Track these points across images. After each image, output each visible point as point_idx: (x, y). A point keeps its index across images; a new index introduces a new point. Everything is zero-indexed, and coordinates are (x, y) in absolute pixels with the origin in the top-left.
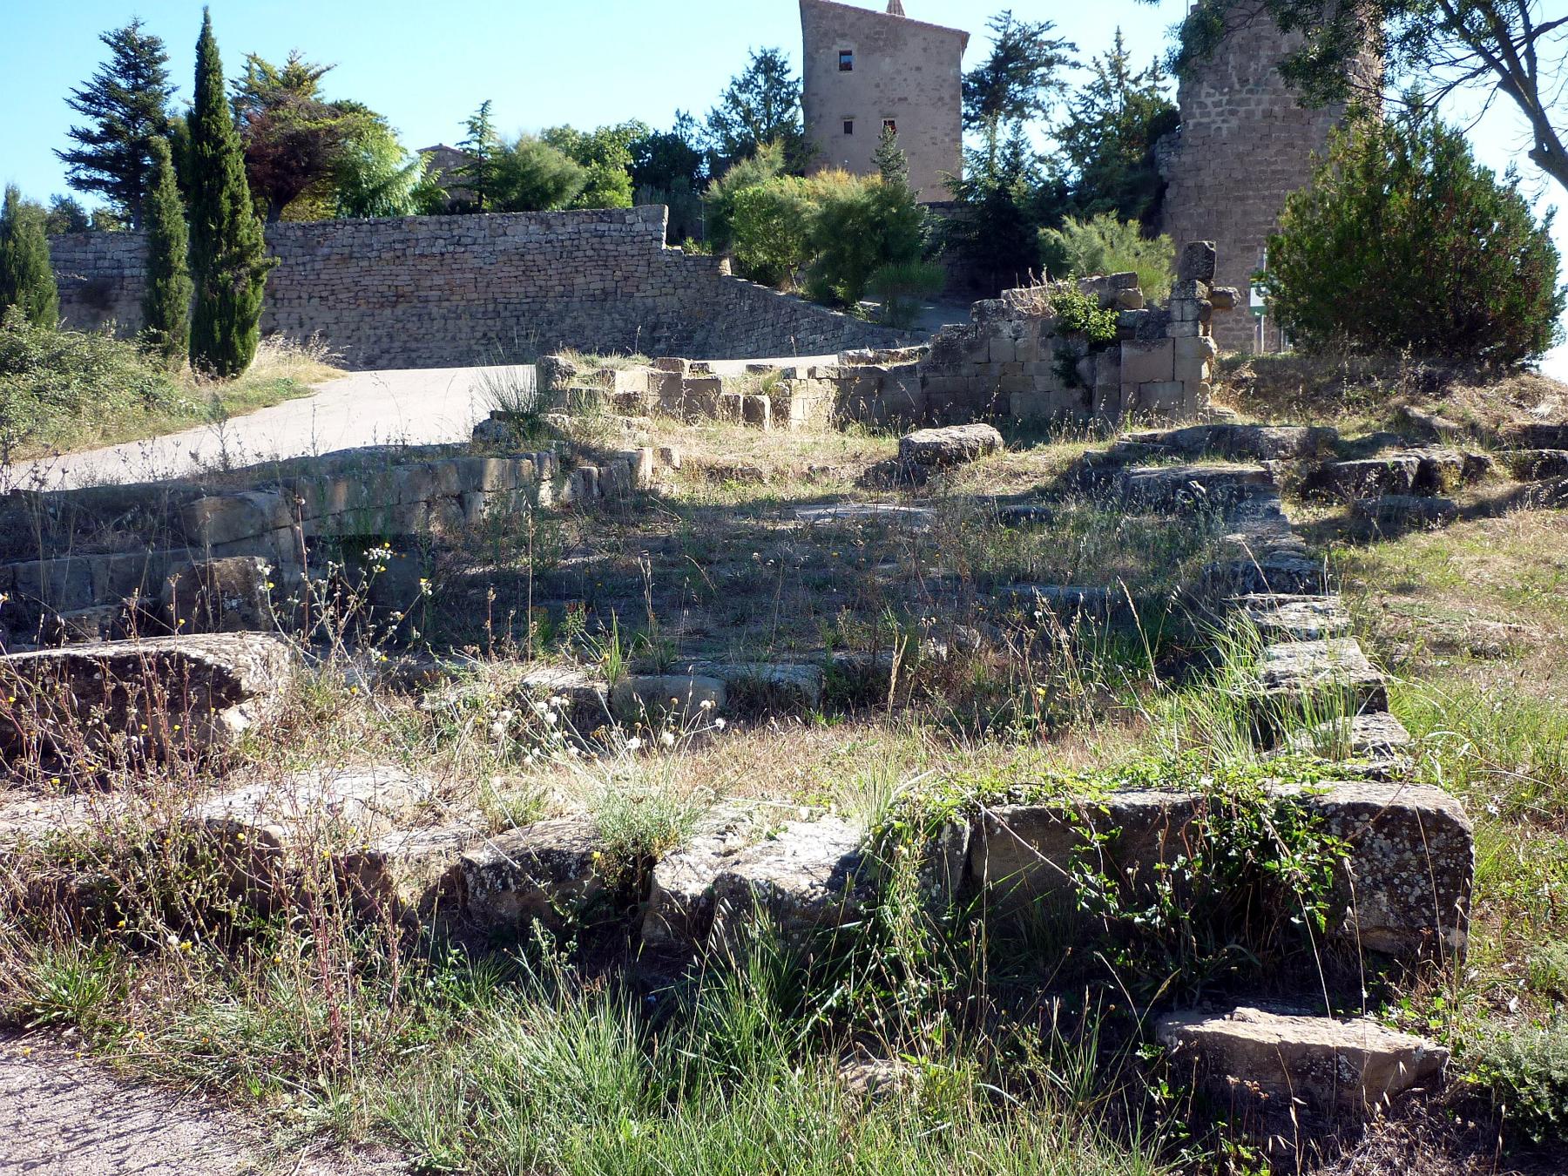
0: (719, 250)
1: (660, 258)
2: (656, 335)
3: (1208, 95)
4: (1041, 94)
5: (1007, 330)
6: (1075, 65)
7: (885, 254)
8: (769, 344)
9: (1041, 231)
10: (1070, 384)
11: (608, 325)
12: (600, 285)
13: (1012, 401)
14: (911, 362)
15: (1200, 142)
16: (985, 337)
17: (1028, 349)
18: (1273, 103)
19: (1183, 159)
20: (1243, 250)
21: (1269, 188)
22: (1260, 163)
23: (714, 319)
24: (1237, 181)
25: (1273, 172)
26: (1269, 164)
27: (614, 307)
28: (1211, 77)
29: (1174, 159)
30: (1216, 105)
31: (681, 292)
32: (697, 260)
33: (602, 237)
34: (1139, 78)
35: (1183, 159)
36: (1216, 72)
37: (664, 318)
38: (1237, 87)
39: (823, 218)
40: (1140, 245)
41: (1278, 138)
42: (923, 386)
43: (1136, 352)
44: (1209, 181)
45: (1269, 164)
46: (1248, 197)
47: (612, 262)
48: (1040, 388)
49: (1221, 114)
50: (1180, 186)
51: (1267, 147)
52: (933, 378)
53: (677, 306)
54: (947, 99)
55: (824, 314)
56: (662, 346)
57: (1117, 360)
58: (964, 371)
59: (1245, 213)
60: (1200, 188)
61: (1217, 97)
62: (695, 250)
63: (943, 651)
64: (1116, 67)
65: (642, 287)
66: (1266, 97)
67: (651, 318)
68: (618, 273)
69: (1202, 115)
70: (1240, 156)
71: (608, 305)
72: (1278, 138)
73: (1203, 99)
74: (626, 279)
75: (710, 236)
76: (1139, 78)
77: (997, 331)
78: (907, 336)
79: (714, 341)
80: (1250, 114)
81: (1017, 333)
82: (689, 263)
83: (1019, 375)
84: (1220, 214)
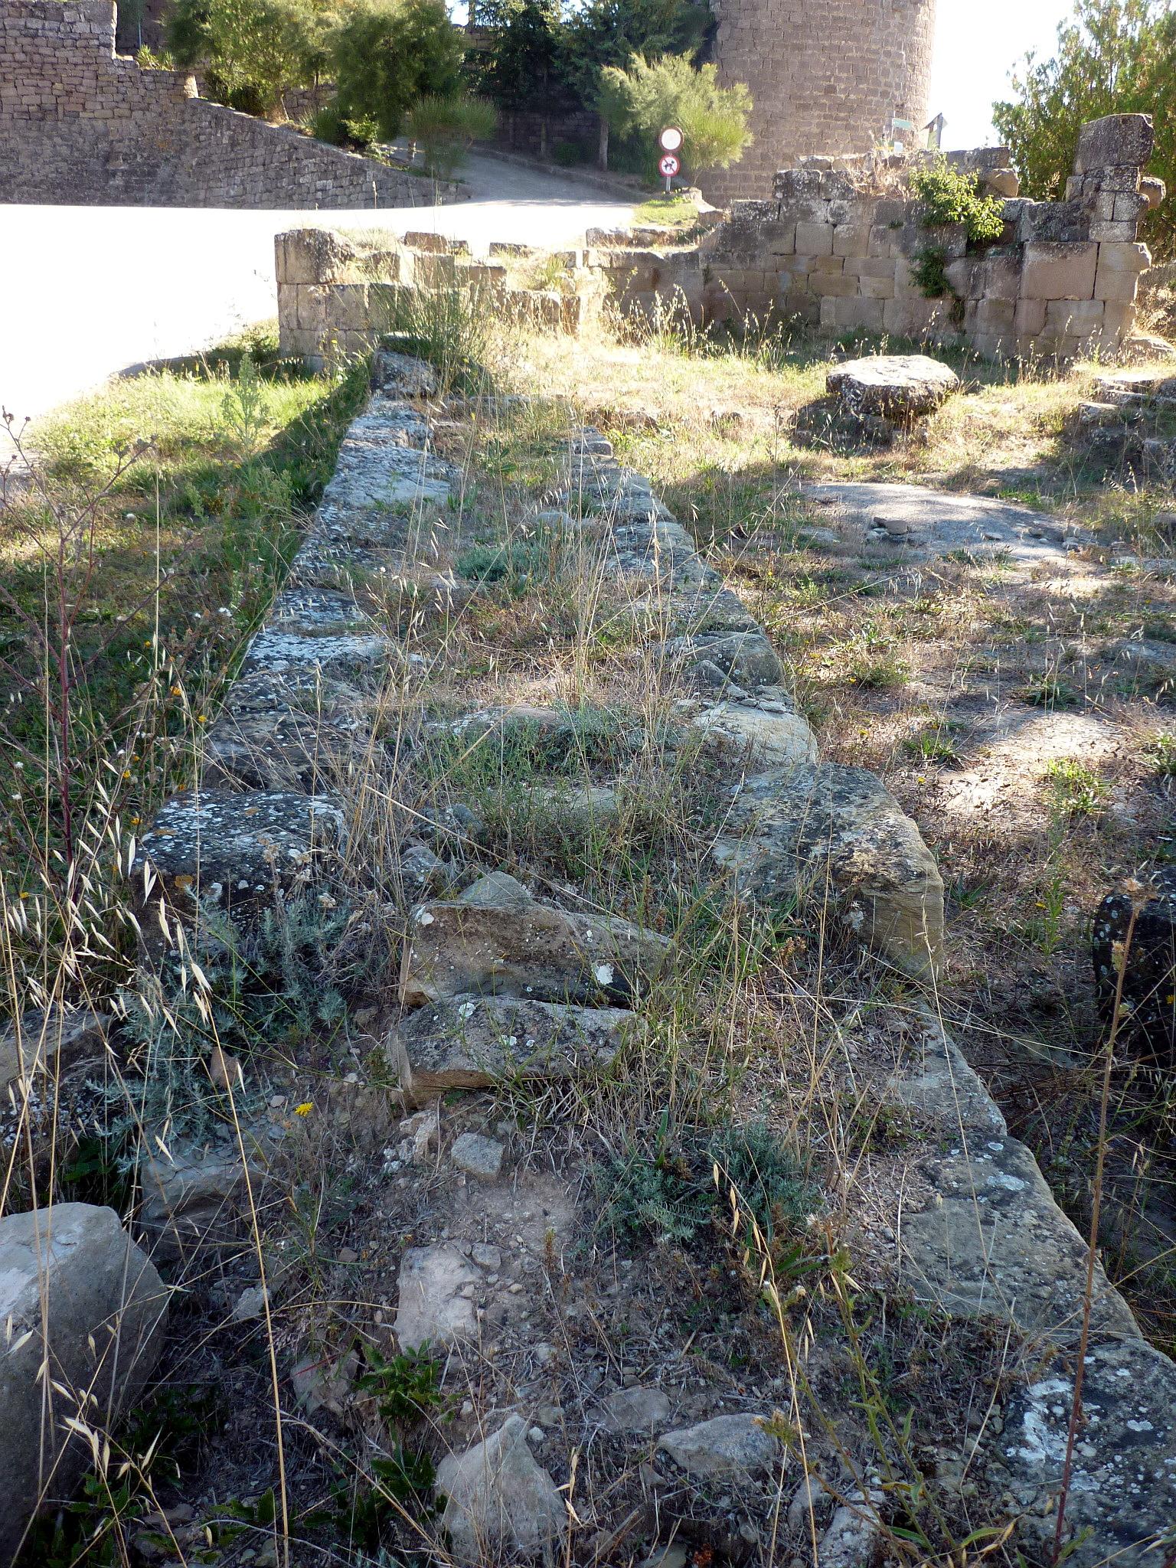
0: (185, 63)
1: (111, 70)
2: (110, 167)
5: (822, 212)
7: (424, 87)
8: (260, 186)
9: (606, 70)
10: (938, 293)
11: (48, 151)
12: (36, 100)
13: (824, 307)
14: (692, 247)
16: (790, 220)
17: (854, 240)
21: (829, 37)
23: (181, 151)
24: (796, 27)
25: (835, 19)
27: (55, 128)
31: (138, 114)
32: (157, 76)
33: (34, 36)
37: (119, 147)
39: (347, 33)
40: (714, 94)
42: (706, 281)
43: (1047, 257)
47: (48, 71)
48: (867, 293)
50: (734, 26)
53: (135, 133)
55: (339, 156)
56: (118, 181)
57: (1016, 267)
58: (761, 263)
60: (755, 30)
62: (152, 61)
65: (88, 105)
67: (103, 146)
68: (58, 85)
71: (48, 124)
74: (69, 93)
75: (173, 48)
77: (808, 213)
78: (452, 189)
79: (182, 178)
81: (838, 218)
82: (147, 79)
83: (837, 274)
84: (777, 64)
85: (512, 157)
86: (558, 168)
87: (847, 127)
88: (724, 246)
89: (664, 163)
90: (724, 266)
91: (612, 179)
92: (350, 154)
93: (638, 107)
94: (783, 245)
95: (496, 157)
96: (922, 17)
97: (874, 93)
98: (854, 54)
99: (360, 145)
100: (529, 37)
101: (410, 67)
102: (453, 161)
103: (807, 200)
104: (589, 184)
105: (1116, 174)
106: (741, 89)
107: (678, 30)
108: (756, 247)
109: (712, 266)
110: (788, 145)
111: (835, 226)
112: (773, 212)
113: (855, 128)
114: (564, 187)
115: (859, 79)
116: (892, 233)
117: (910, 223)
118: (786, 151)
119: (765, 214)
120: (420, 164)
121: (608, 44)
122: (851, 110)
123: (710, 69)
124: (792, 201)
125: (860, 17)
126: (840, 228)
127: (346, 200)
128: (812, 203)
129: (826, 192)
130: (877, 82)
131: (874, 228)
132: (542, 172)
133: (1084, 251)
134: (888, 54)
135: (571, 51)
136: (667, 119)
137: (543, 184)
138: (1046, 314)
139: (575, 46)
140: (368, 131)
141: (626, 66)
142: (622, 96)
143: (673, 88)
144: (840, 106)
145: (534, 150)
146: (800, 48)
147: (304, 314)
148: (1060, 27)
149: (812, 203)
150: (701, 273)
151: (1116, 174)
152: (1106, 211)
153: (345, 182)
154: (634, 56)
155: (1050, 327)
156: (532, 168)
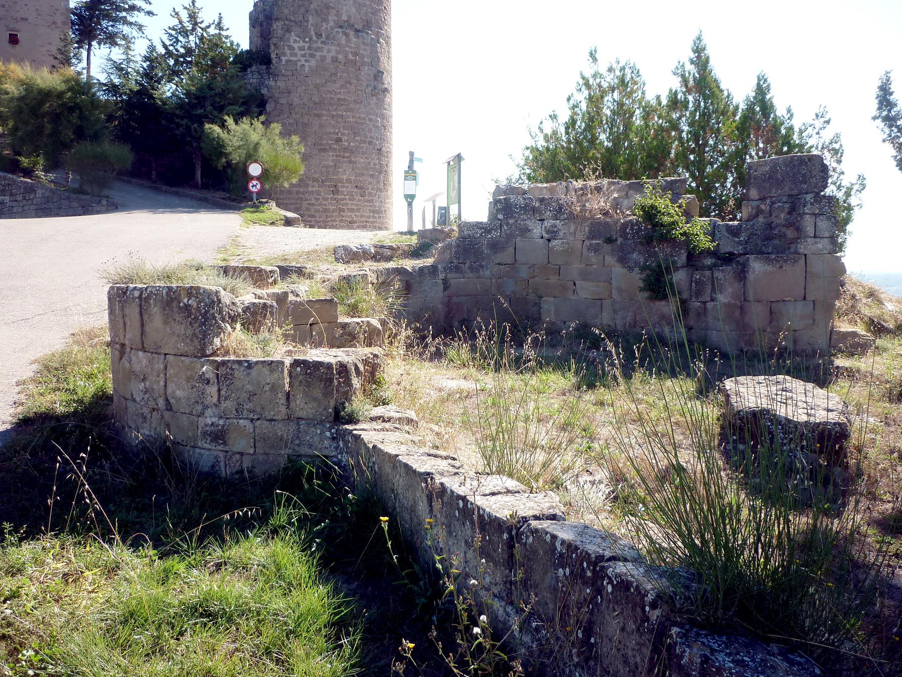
3: (295, 41)
4: (126, 29)
5: (537, 230)
6: (150, 13)
7: (80, 134)
9: (207, 126)
13: (545, 306)
15: (290, 73)
18: (338, 52)
19: (279, 84)
20: (320, 150)
21: (336, 110)
22: (330, 92)
24: (315, 103)
25: (339, 99)
26: (336, 93)
28: (297, 29)
29: (272, 83)
30: (301, 49)
34: (209, 27)
35: (279, 84)
36: (300, 26)
38: (314, 38)
39: (21, 99)
40: (279, 142)
41: (341, 77)
42: (445, 289)
43: (769, 268)
44: (296, 101)
45: (336, 93)
46: (323, 115)
49: (304, 56)
50: (277, 102)
51: (335, 82)
52: (456, 280)
54: (59, 23)
55: (14, 181)
57: (742, 274)
59: (321, 126)
61: (301, 44)
63: (675, 630)
64: (193, 17)
66: (333, 48)
69: (291, 55)
70: (317, 86)
72: (341, 77)
73: (292, 44)
76: (209, 27)
77: (526, 230)
80: (323, 59)
81: (553, 234)
83: (553, 279)
85: (134, 180)
86: (168, 188)
87: (350, 162)
88: (458, 258)
89: (251, 185)
90: (458, 275)
91: (209, 195)
92: (22, 179)
93: (229, 149)
94: (506, 257)
95: (123, 181)
96: (387, 100)
97: (365, 142)
98: (351, 120)
99: (28, 173)
100: (141, 106)
101: (69, 122)
102: (103, 184)
103: (524, 220)
104: (193, 197)
105: (816, 201)
106: (295, 139)
107: (243, 104)
108: (483, 259)
109: (449, 276)
110: (315, 172)
111: (549, 240)
112: (496, 230)
113: (355, 162)
114: (176, 200)
115: (355, 134)
116: (607, 248)
117: (626, 239)
118: (314, 176)
119: (489, 232)
120: (77, 186)
121: (200, 111)
122: (352, 152)
123: (276, 127)
124: (511, 221)
125: (353, 99)
126: (554, 243)
127: (20, 210)
128: (528, 223)
129: (540, 213)
130: (366, 136)
131: (587, 243)
132: (157, 190)
133: (796, 262)
134: (371, 120)
135: (174, 114)
136: (251, 157)
137: (161, 198)
138: (771, 312)
139: (177, 112)
140: (35, 164)
141: (223, 125)
142: (218, 143)
143: (254, 137)
144: (345, 149)
145: (148, 176)
146: (318, 116)
147: (179, 393)
148: (569, 99)
149: (528, 223)
150: (440, 282)
151: (816, 201)
152: (810, 230)
153: (20, 198)
154: (226, 117)
155: (775, 323)
156: (150, 187)
